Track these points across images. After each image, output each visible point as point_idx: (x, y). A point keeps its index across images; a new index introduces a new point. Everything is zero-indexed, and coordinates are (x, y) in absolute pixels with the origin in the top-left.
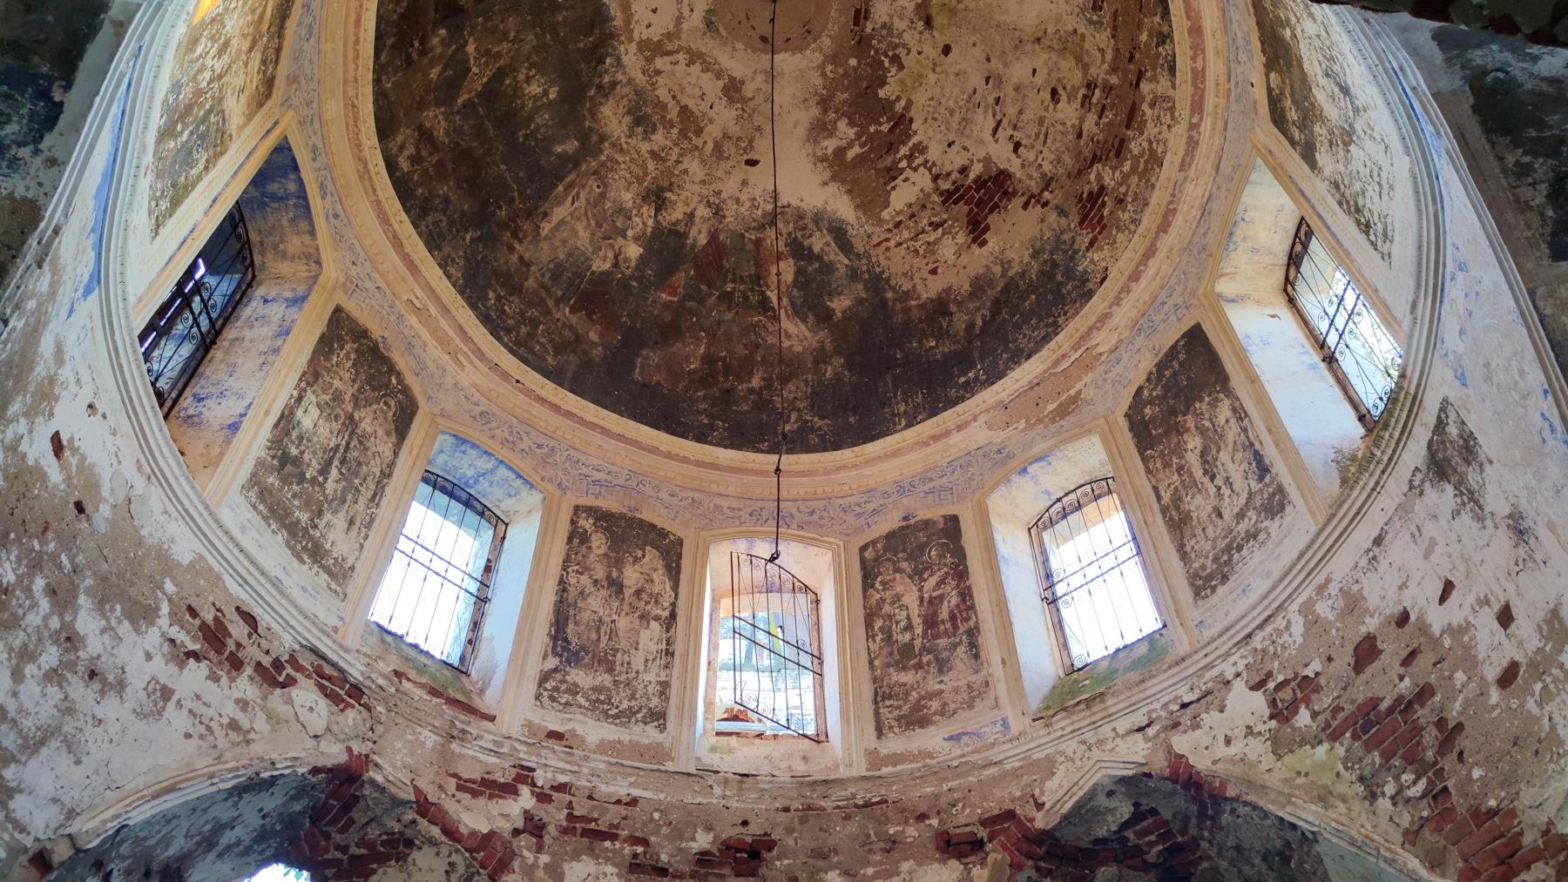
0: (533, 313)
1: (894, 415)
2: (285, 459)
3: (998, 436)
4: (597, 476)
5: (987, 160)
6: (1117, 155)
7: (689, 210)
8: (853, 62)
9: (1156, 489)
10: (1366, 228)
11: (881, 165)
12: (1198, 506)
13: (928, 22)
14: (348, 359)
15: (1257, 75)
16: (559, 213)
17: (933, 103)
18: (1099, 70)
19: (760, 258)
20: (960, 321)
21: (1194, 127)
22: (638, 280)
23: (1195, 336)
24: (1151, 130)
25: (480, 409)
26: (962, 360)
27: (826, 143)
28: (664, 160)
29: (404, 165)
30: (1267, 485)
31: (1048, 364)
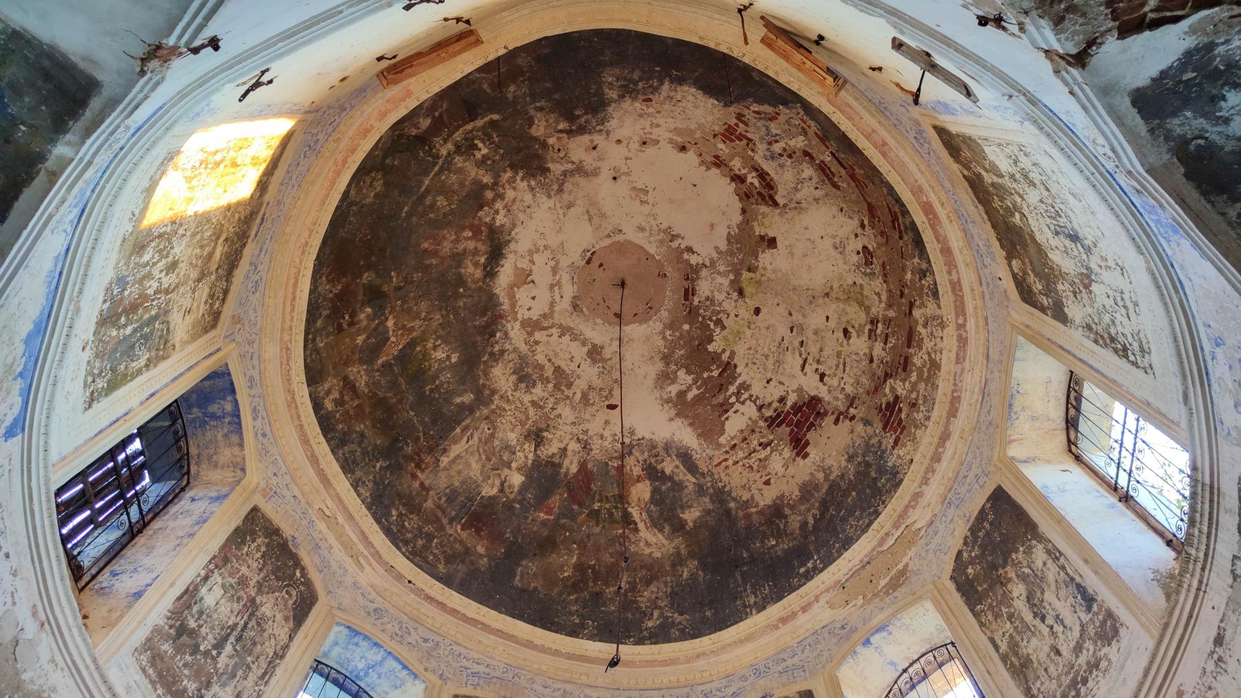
0: (429, 528)
1: (745, 606)
2: (182, 630)
3: (840, 614)
4: (477, 668)
5: (800, 390)
6: (904, 370)
7: (562, 446)
8: (686, 327)
9: (992, 640)
10: (1123, 352)
11: (715, 402)
12: (1037, 648)
13: (741, 293)
14: (258, 550)
15: (1002, 271)
16: (456, 450)
17: (752, 352)
18: (878, 309)
19: (623, 480)
20: (794, 522)
21: (961, 327)
22: (520, 502)
23: (999, 497)
24: (928, 344)
25: (375, 606)
26: (801, 553)
27: (670, 388)
28: (542, 408)
29: (329, 405)
30: (1097, 614)
31: (875, 542)
